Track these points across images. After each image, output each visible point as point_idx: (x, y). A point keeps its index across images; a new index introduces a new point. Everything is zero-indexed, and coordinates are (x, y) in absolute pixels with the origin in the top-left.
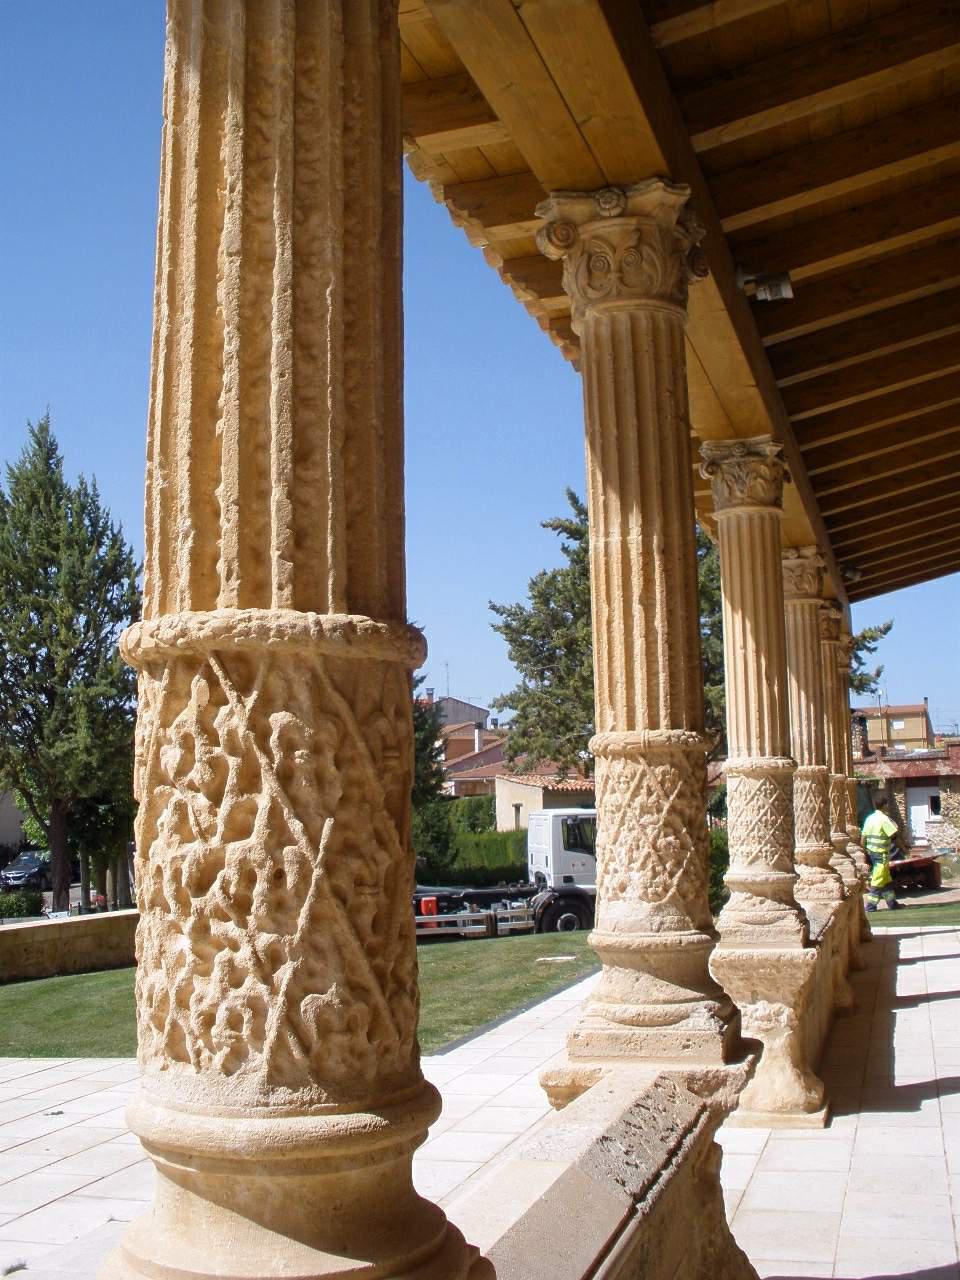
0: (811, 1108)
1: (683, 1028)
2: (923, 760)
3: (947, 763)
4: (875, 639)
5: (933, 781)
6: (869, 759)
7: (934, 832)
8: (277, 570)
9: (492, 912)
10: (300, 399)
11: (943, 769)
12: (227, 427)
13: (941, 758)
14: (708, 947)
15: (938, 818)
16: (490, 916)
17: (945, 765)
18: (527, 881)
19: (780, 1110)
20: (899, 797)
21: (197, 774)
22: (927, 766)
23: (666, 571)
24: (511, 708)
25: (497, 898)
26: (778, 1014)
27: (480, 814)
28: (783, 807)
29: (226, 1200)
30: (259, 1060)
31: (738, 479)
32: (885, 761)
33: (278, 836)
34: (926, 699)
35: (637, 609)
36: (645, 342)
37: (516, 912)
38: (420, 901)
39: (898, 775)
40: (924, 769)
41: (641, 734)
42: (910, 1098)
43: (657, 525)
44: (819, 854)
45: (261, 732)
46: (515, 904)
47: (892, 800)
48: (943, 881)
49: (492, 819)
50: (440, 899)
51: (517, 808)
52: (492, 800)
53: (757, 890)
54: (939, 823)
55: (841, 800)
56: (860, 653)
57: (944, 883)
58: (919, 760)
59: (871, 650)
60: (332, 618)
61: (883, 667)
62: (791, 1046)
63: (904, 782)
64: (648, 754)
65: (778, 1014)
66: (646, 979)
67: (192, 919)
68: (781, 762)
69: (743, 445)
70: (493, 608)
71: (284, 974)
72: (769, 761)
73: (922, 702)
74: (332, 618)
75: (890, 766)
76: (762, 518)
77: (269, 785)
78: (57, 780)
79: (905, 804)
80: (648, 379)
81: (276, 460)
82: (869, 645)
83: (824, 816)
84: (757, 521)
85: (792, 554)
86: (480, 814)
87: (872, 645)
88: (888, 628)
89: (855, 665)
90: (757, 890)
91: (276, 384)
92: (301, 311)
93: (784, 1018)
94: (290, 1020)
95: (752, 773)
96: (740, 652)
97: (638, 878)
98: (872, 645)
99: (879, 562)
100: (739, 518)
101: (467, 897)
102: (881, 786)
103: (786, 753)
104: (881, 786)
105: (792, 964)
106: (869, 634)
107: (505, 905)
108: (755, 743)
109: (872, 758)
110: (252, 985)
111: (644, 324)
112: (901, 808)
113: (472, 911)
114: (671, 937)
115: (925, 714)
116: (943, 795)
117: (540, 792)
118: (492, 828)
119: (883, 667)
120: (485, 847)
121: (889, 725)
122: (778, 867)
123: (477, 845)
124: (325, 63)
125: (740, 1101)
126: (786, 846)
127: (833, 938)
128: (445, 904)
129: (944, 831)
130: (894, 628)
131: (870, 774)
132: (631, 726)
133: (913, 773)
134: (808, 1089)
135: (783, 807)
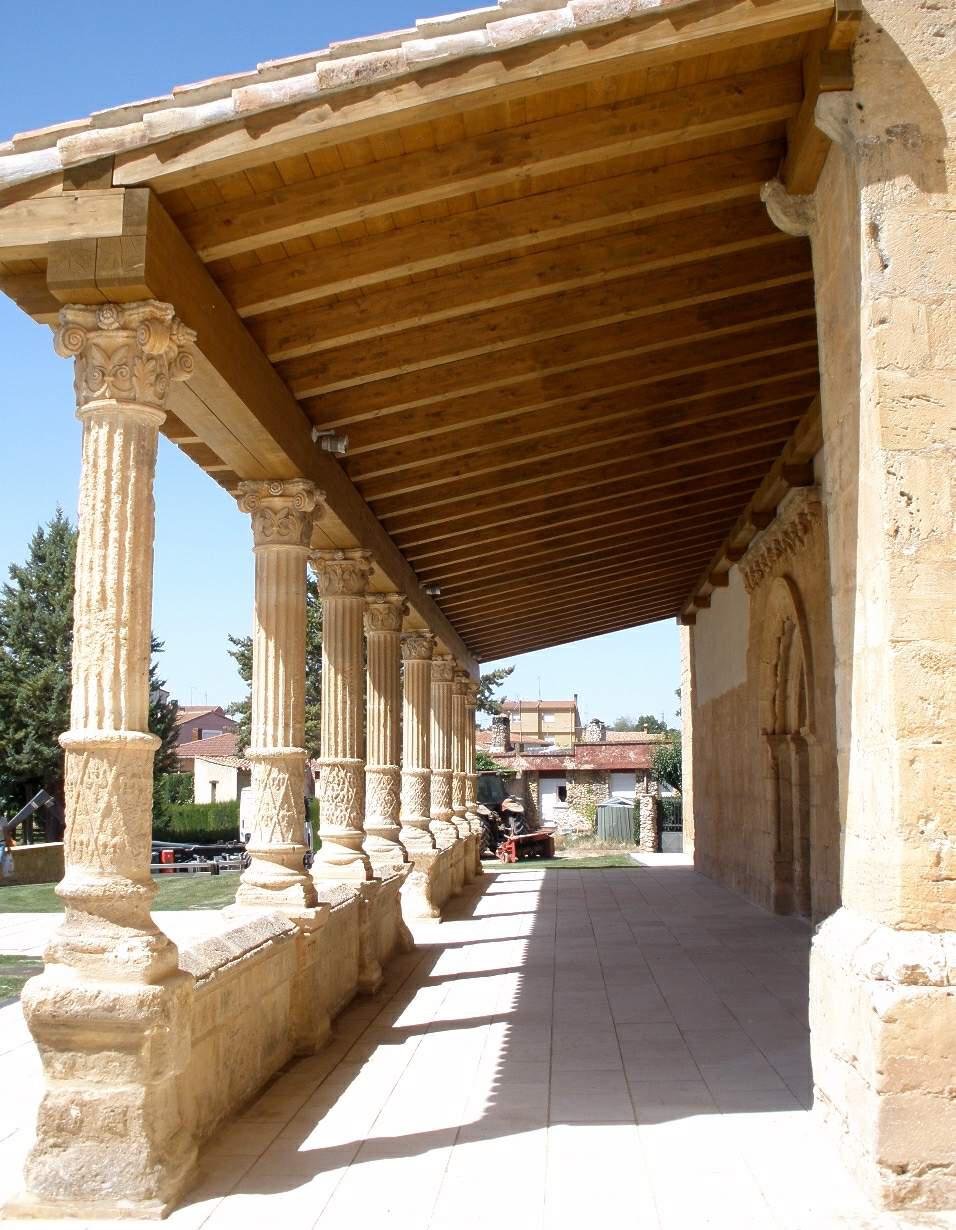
0: (434, 917)
1: (391, 853)
4: (502, 678)
5: (560, 774)
6: (510, 753)
7: (561, 815)
8: (348, 752)
9: (214, 862)
10: (351, 726)
11: (569, 765)
12: (340, 730)
14: (399, 830)
15: (565, 804)
16: (214, 865)
18: (238, 838)
19: (421, 917)
20: (533, 786)
21: (336, 781)
22: (557, 761)
23: (391, 717)
24: (241, 712)
25: (218, 852)
26: (422, 877)
27: (181, 789)
28: (426, 789)
29: (340, 843)
30: (345, 823)
31: (414, 648)
32: (522, 756)
33: (348, 791)
34: (576, 696)
35: (382, 729)
36: (389, 644)
37: (232, 863)
38: (160, 853)
39: (533, 768)
41: (382, 766)
42: (479, 918)
43: (389, 702)
44: (446, 815)
45: (346, 776)
46: (232, 857)
47: (527, 789)
48: (556, 852)
49: (191, 793)
50: (176, 851)
51: (214, 784)
52: (191, 776)
53: (414, 825)
55: (462, 788)
56: (491, 686)
57: (557, 854)
58: (550, 756)
60: (356, 760)
62: (427, 891)
63: (537, 774)
64: (384, 772)
65: (422, 877)
66: (381, 839)
68: (426, 770)
69: (417, 632)
70: (232, 640)
71: (349, 811)
72: (421, 770)
73: (573, 699)
74: (356, 760)
76: (423, 665)
77: (347, 784)
79: (538, 791)
80: (389, 656)
81: (348, 736)
83: (449, 795)
84: (421, 667)
85: (439, 658)
86: (181, 789)
87: (500, 681)
88: (511, 671)
89: (487, 694)
90: (414, 825)
91: (348, 724)
92: (352, 712)
93: (424, 879)
94: (349, 817)
95: (414, 775)
96: (410, 723)
97: (379, 809)
98: (500, 681)
99: (583, 504)
100: (413, 664)
101: (196, 851)
102: (518, 777)
103: (428, 767)
104: (518, 777)
105: (427, 856)
107: (225, 858)
108: (415, 762)
109: (512, 753)
110: (344, 812)
111: (389, 638)
112: (534, 795)
113: (201, 861)
114: (389, 826)
115: (575, 710)
116: (568, 786)
117: (235, 772)
118: (190, 801)
120: (188, 816)
121: (540, 719)
122: (423, 815)
123: (181, 814)
124: (347, 664)
126: (426, 806)
127: (452, 858)
128: (179, 856)
131: (509, 766)
132: (379, 763)
134: (433, 909)
135: (426, 789)
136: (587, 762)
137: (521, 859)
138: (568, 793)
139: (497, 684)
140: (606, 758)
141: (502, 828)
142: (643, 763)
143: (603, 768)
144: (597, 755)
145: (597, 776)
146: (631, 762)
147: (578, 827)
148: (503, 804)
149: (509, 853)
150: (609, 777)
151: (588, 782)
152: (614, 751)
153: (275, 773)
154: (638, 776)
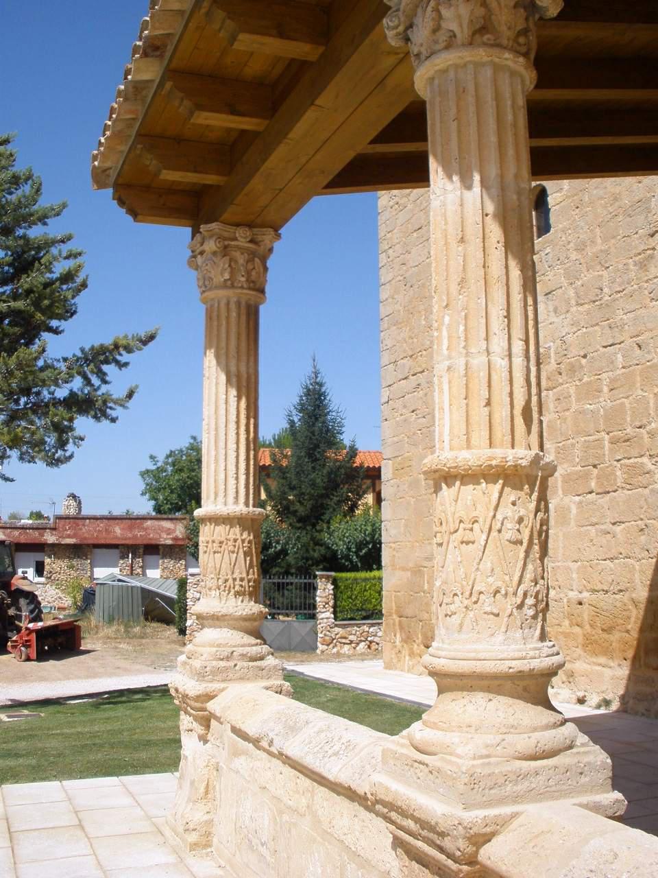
2: (33, 529)
3: (54, 533)
4: (129, 350)
5: (39, 547)
11: (50, 538)
13: (50, 529)
15: (42, 580)
17: (52, 535)
40: (34, 536)
54: (43, 584)
56: (105, 368)
58: (29, 529)
59: (122, 365)
61: (137, 387)
67: (589, 379)
75: (4, 533)
78: (565, 600)
82: (118, 357)
83: (589, 441)
98: (124, 357)
106: (124, 342)
116: (47, 560)
119: (137, 387)
125: (494, 840)
129: (46, 592)
130: (157, 339)
133: (23, 540)
136: (69, 536)
137: (42, 656)
138: (47, 568)
139: (117, 363)
140: (89, 533)
141: (11, 612)
142: (130, 538)
143: (86, 542)
144: (81, 529)
145: (78, 551)
146: (117, 538)
147: (56, 604)
148: (12, 581)
149: (27, 647)
150: (91, 552)
151: (69, 557)
152: (98, 526)
153: (245, 535)
154: (121, 552)
